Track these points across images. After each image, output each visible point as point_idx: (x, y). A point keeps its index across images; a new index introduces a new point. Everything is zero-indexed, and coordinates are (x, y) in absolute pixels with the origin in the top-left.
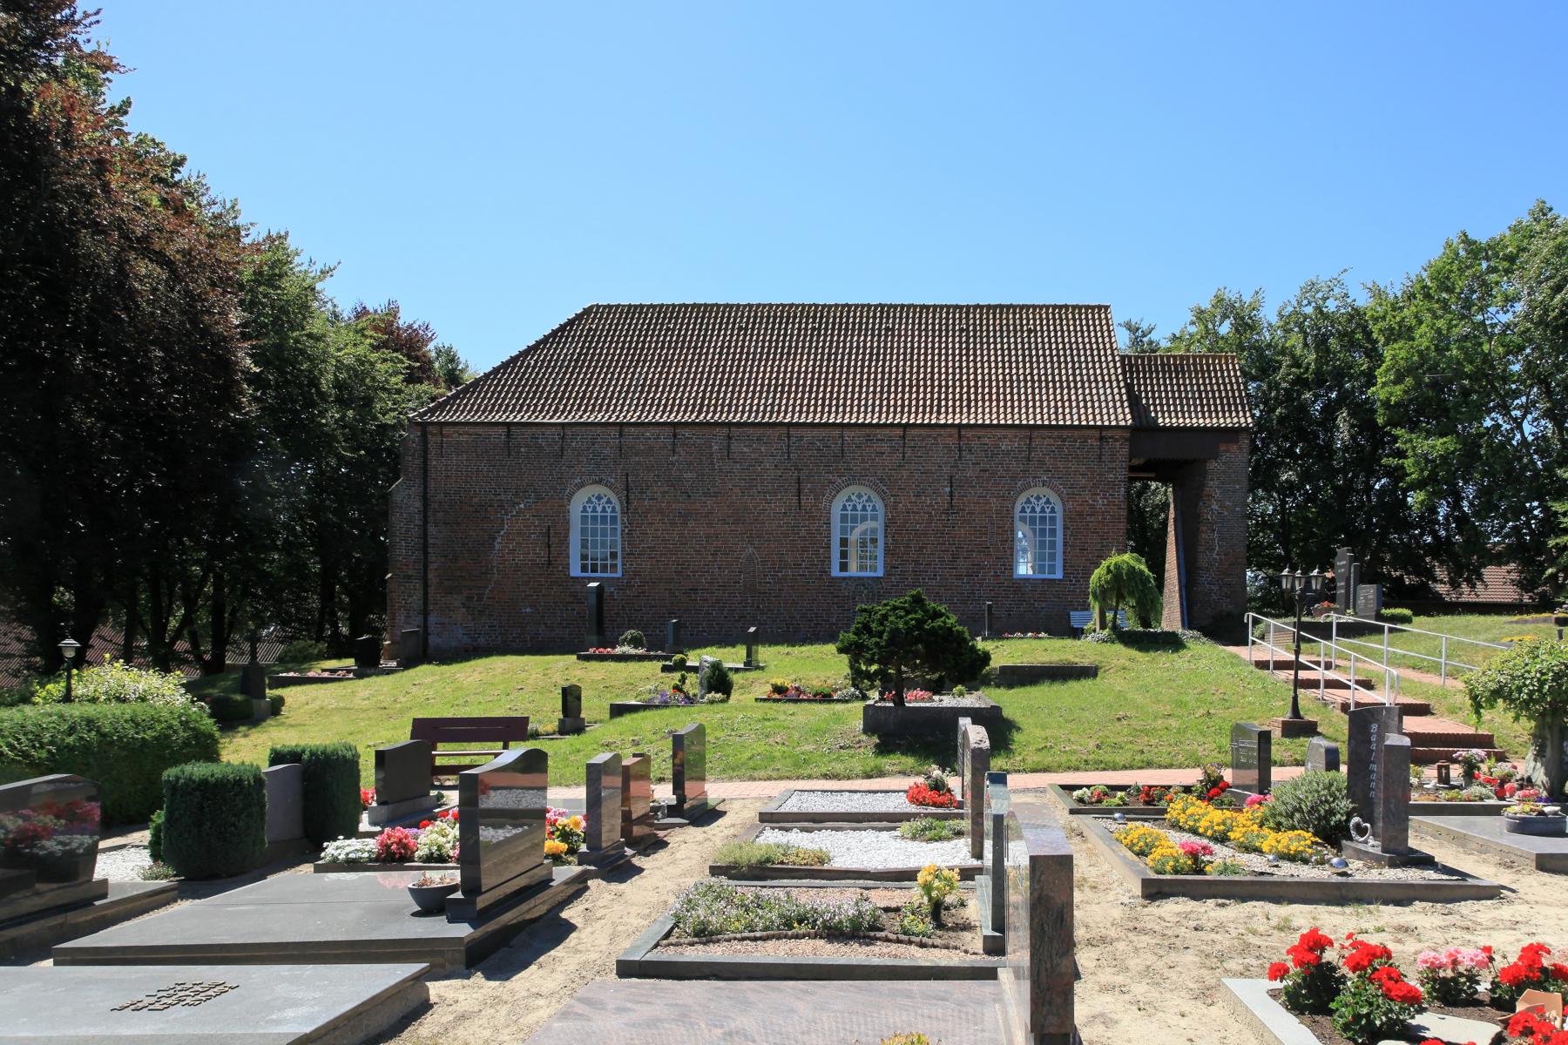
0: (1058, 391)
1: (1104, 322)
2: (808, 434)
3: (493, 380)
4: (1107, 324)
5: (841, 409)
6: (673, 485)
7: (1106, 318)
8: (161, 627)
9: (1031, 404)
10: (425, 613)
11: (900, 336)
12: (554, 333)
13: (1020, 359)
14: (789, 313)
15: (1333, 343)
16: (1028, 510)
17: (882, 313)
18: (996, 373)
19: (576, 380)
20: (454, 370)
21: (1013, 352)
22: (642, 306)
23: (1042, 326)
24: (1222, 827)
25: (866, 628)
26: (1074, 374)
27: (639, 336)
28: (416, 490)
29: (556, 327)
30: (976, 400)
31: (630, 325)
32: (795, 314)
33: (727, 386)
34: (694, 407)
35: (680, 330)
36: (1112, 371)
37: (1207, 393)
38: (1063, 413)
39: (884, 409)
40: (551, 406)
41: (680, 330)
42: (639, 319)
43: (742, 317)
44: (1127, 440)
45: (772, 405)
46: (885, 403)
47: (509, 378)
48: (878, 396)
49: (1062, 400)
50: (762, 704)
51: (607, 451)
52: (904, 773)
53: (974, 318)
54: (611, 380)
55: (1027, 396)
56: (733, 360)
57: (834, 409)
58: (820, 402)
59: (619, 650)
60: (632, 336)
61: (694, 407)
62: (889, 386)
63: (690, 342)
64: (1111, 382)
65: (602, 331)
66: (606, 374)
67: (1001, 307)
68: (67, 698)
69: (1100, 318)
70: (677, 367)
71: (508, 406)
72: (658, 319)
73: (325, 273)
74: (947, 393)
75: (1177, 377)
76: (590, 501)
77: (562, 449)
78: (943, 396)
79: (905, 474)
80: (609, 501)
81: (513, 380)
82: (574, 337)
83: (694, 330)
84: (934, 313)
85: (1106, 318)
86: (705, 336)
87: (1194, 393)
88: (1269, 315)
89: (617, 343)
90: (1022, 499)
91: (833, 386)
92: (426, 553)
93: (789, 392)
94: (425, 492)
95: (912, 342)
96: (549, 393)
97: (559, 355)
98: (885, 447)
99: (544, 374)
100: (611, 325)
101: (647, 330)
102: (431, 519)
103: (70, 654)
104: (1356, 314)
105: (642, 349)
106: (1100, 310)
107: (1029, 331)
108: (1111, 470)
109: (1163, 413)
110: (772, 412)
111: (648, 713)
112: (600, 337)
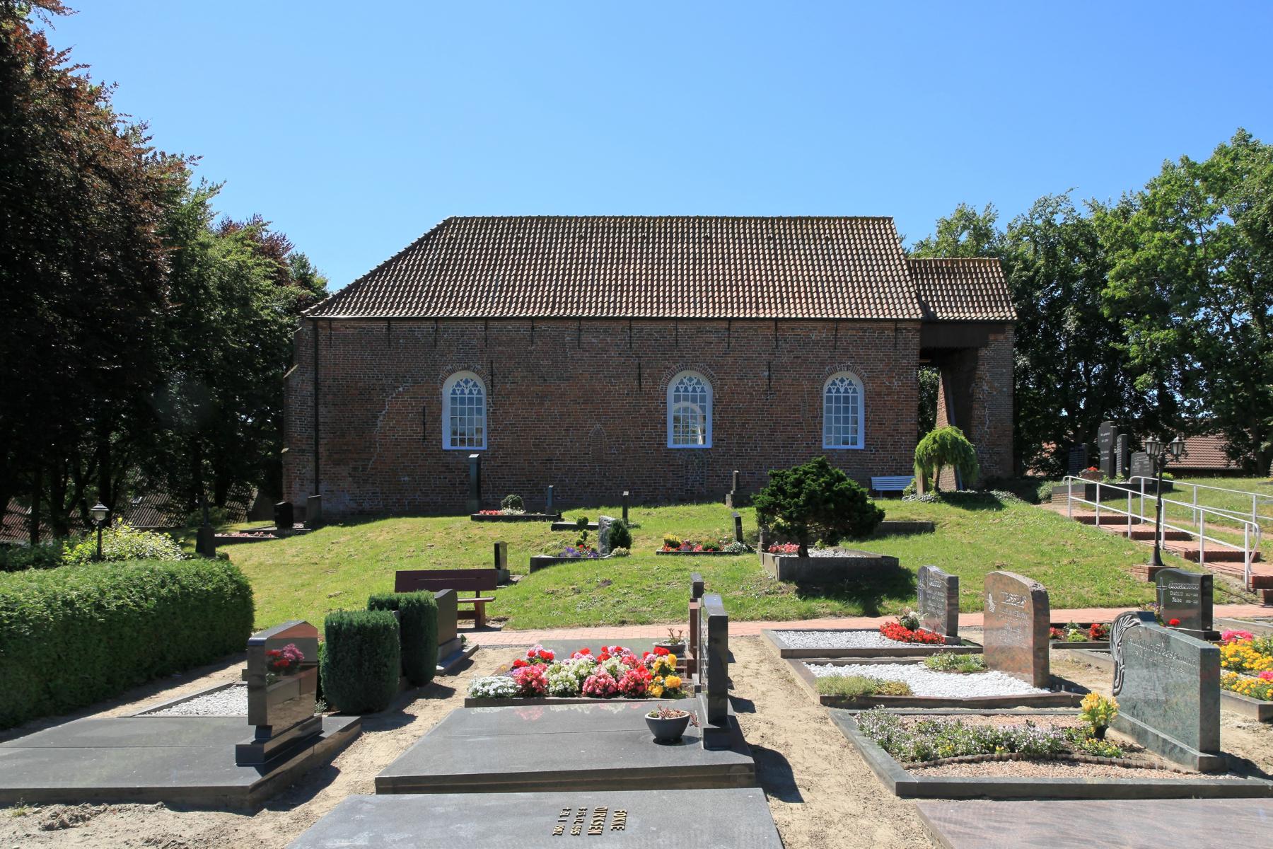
0: (857, 290)
1: (889, 231)
2: (648, 326)
3: (372, 281)
4: (892, 233)
5: (674, 305)
6: (531, 371)
7: (891, 228)
8: (58, 498)
9: (834, 301)
10: (317, 482)
11: (717, 244)
12: (420, 242)
13: (821, 262)
14: (621, 225)
15: (1061, 250)
16: (834, 391)
17: (700, 224)
18: (802, 275)
19: (444, 281)
20: (306, 274)
21: (762, 262)
22: (494, 219)
23: (837, 235)
24: (1237, 659)
25: (781, 490)
26: (868, 275)
27: (494, 244)
28: (309, 375)
29: (421, 236)
30: (788, 298)
31: (485, 234)
32: (626, 225)
33: (574, 286)
34: (548, 304)
35: (529, 239)
36: (805, 273)
37: (976, 291)
38: (863, 308)
39: (711, 305)
40: (424, 303)
41: (529, 239)
42: (492, 229)
43: (581, 227)
44: (918, 331)
45: (615, 301)
46: (710, 300)
47: (386, 279)
48: (704, 294)
49: (860, 297)
50: (663, 557)
51: (474, 342)
52: (833, 614)
53: (779, 228)
54: (473, 281)
55: (830, 294)
56: (577, 264)
57: (667, 305)
58: (655, 300)
59: (500, 513)
60: (488, 244)
61: (548, 304)
62: (713, 285)
63: (538, 249)
64: (900, 282)
65: (461, 239)
66: (469, 276)
67: (801, 219)
68: (98, 557)
69: (885, 228)
70: (529, 270)
71: (386, 303)
72: (508, 229)
73: (214, 190)
74: (762, 292)
75: (949, 278)
76: (458, 385)
78: (759, 294)
79: (730, 360)
80: (475, 385)
81: (389, 282)
82: (437, 245)
83: (540, 238)
84: (744, 223)
85: (891, 228)
86: (551, 244)
87: (965, 291)
88: (1000, 227)
89: (476, 249)
90: (829, 382)
91: (664, 285)
92: (317, 431)
93: (628, 291)
94: (316, 379)
95: (728, 248)
96: (421, 292)
97: (427, 260)
98: (713, 338)
99: (415, 276)
100: (468, 234)
101: (501, 239)
102: (321, 401)
103: (100, 517)
104: (1081, 226)
105: (498, 255)
106: (884, 221)
107: (827, 239)
108: (904, 357)
109: (941, 308)
110: (615, 308)
111: (559, 567)
112: (460, 244)
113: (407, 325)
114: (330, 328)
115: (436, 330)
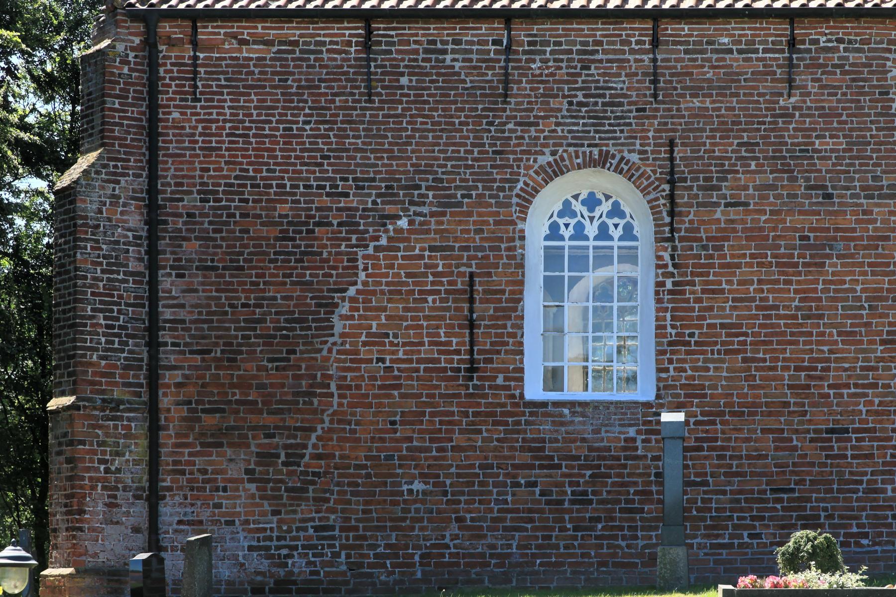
51: (619, 84)
77: (506, 81)
92: (154, 345)
94: (152, 190)
102: (166, 258)
113: (421, 33)
114: (195, 44)
115: (508, 50)
